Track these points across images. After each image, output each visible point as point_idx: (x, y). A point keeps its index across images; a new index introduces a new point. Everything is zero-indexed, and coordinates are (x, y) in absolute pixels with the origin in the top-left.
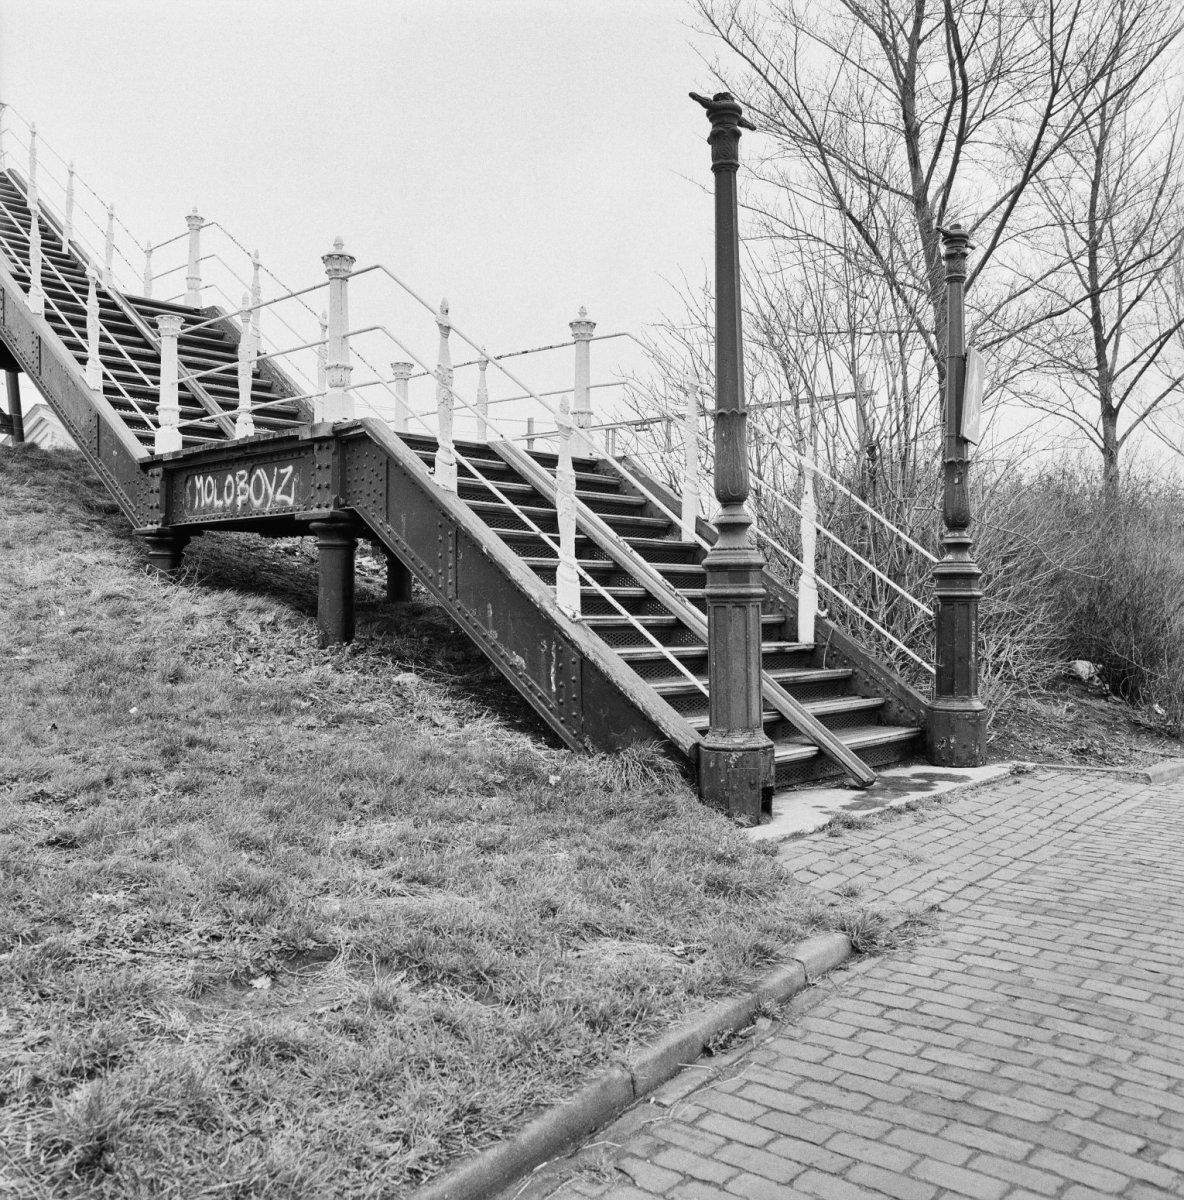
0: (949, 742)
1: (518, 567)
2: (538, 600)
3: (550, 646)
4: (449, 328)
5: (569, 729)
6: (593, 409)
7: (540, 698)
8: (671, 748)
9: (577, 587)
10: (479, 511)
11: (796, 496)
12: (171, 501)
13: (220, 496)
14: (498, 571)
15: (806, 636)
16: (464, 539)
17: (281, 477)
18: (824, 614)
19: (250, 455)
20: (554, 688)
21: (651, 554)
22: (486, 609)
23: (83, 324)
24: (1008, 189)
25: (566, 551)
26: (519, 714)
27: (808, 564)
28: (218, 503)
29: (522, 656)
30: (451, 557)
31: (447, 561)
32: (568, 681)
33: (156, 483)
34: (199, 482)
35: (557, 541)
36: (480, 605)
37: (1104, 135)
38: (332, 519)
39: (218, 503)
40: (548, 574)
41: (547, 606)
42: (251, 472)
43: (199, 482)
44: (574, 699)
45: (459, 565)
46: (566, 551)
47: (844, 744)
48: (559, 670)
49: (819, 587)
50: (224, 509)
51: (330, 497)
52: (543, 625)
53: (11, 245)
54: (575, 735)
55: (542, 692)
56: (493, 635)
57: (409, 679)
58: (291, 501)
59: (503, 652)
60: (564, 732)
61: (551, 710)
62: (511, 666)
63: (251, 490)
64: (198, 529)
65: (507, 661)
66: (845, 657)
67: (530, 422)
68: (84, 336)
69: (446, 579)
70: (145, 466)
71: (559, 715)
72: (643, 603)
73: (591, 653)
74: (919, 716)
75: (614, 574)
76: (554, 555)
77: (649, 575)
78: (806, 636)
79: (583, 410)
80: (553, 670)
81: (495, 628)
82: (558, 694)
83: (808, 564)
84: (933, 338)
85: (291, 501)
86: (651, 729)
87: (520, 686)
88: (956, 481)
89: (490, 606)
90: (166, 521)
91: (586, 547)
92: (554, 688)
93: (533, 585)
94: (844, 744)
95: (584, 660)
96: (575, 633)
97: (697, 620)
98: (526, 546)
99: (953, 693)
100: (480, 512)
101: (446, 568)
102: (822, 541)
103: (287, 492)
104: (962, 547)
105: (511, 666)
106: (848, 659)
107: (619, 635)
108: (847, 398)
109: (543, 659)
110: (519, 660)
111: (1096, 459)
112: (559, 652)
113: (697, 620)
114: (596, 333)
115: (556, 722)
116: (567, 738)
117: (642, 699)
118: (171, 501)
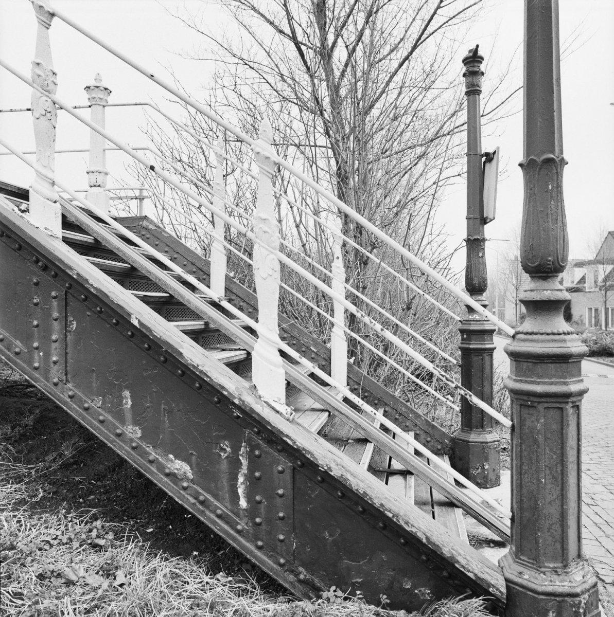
0: (483, 468)
2: (236, 394)
3: (236, 449)
4: (53, 15)
5: (270, 557)
6: (108, 171)
7: (219, 516)
18: (352, 360)
20: (243, 503)
22: (121, 398)
24: (419, 47)
29: (187, 460)
30: (56, 325)
31: (49, 332)
32: (271, 496)
36: (110, 391)
41: (250, 400)
44: (282, 519)
45: (69, 337)
48: (253, 484)
54: (281, 565)
55: (222, 508)
56: (134, 432)
59: (153, 455)
60: (286, 579)
61: (238, 532)
62: (167, 475)
65: (161, 468)
66: (375, 398)
69: (47, 355)
71: (254, 538)
73: (333, 466)
74: (443, 443)
79: (100, 169)
80: (241, 479)
81: (136, 423)
82: (252, 512)
87: (187, 501)
88: (480, 255)
89: (127, 393)
92: (243, 503)
99: (482, 427)
101: (46, 339)
105: (167, 475)
106: (379, 400)
108: (132, 199)
109: (224, 466)
110: (179, 466)
112: (254, 463)
114: (111, 99)
116: (272, 569)
117: (423, 528)
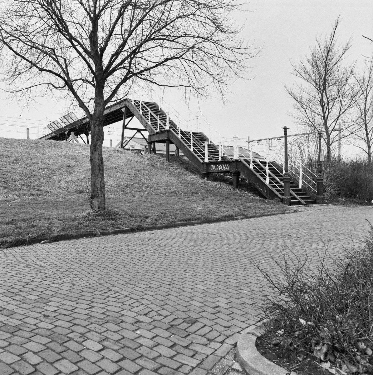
1: (261, 178)
8: (280, 198)
9: (269, 181)
10: (255, 171)
11: (299, 167)
12: (207, 169)
13: (216, 168)
14: (259, 179)
15: (300, 187)
16: (193, 155)
17: (226, 166)
19: (221, 163)
21: (277, 176)
23: (190, 141)
25: (267, 176)
26: (261, 196)
27: (301, 178)
28: (216, 169)
33: (205, 166)
34: (212, 166)
35: (266, 175)
37: (367, 96)
38: (236, 172)
39: (216, 169)
40: (265, 179)
42: (221, 165)
43: (212, 166)
46: (267, 176)
47: (302, 201)
49: (302, 181)
50: (217, 170)
51: (235, 169)
52: (265, 185)
53: (197, 138)
56: (258, 187)
57: (246, 192)
58: (228, 169)
60: (267, 198)
63: (221, 167)
64: (211, 173)
67: (249, 137)
68: (190, 143)
70: (203, 164)
72: (277, 183)
75: (273, 179)
76: (266, 177)
77: (277, 179)
78: (300, 187)
83: (301, 178)
84: (326, 139)
85: (228, 169)
86: (277, 196)
90: (207, 171)
91: (270, 175)
93: (264, 181)
94: (302, 201)
95: (270, 189)
96: (268, 186)
97: (283, 184)
98: (262, 175)
100: (255, 171)
102: (303, 175)
103: (227, 168)
104: (321, 175)
107: (274, 187)
111: (367, 156)
113: (283, 184)
115: (266, 197)
118: (207, 169)
